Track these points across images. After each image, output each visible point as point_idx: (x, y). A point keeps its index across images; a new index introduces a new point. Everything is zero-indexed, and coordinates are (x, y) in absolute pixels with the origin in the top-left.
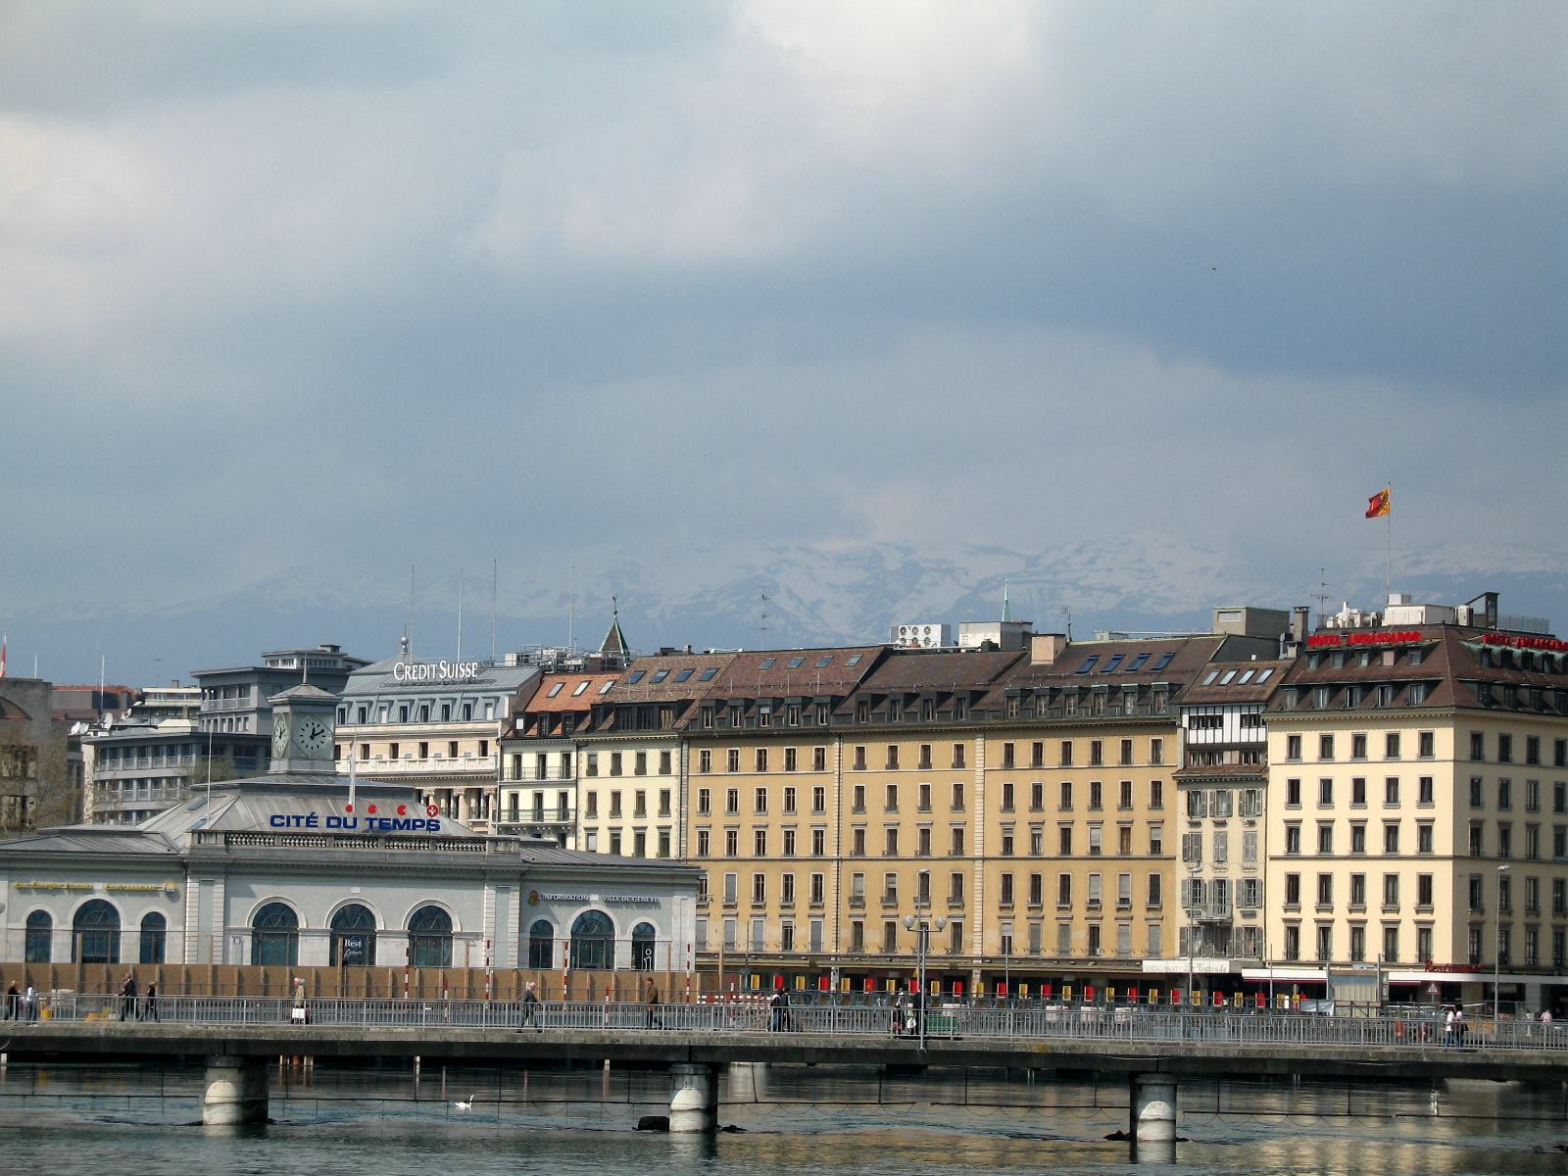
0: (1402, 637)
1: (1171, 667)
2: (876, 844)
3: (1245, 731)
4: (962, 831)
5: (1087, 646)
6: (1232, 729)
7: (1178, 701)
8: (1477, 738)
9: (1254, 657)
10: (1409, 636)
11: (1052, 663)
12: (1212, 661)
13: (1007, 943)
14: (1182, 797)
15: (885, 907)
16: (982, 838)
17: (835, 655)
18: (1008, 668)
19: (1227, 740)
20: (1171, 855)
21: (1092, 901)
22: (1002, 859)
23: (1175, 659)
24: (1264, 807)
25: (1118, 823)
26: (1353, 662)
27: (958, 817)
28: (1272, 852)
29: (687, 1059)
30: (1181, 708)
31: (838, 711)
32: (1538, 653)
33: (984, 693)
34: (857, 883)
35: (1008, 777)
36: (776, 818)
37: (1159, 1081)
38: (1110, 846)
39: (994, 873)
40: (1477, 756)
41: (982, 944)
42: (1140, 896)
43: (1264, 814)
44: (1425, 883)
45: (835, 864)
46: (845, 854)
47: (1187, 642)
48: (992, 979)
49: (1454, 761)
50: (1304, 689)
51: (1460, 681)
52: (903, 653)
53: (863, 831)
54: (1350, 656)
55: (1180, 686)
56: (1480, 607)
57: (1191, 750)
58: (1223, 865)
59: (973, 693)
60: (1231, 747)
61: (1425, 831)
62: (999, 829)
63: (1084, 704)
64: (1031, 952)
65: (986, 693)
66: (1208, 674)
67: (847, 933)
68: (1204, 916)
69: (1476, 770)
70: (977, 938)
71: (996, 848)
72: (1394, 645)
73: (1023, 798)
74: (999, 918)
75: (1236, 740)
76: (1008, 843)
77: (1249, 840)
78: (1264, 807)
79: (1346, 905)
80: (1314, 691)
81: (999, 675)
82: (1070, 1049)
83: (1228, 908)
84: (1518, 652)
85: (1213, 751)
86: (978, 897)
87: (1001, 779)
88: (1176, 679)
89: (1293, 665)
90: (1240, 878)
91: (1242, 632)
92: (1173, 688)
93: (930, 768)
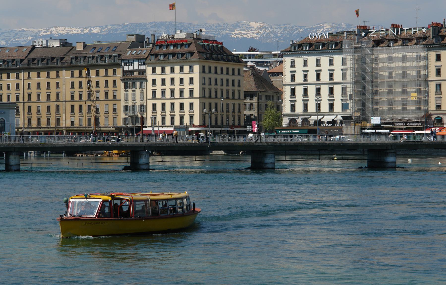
0: (182, 41)
1: (117, 50)
2: (34, 98)
3: (140, 66)
4: (59, 94)
5: (92, 45)
6: (136, 66)
7: (120, 59)
8: (204, 67)
9: (139, 47)
10: (184, 41)
11: (82, 49)
12: (129, 48)
13: (72, 123)
14: (122, 85)
15: (37, 115)
16: (65, 95)
17: (19, 48)
18: (69, 51)
19: (135, 69)
20: (120, 99)
21: (106, 111)
22: (113, 100)
23: (118, 48)
24: (146, 86)
25: (56, 92)
26: (169, 48)
27: (58, 91)
28: (148, 98)
29: (143, 150)
30: (122, 61)
31: (22, 63)
32: (215, 45)
33: (64, 58)
34: (106, 107)
35: (72, 80)
36: (177, 87)
37: (271, 153)
38: (102, 97)
39: (69, 105)
40: (204, 71)
41: (65, 123)
42: (111, 111)
43: (146, 88)
44: (191, 105)
45: (23, 104)
46: (26, 101)
47: (120, 44)
48: (68, 132)
49: (199, 73)
50: (156, 55)
51: (199, 53)
52: (38, 48)
53: (40, 94)
54: (168, 46)
55: (120, 55)
56: (198, 33)
57: (124, 72)
58: (143, 101)
59: (42, 58)
60: (136, 71)
61: (191, 92)
62: (70, 93)
63: (93, 60)
64: (80, 125)
65: (64, 58)
66: (128, 51)
67: (26, 122)
68: (129, 115)
69: (204, 75)
70: (64, 122)
71: (69, 99)
72: (173, 44)
73: (76, 85)
74: (113, 116)
75: (137, 69)
76: (72, 97)
77: (142, 95)
78: (146, 86)
79: (179, 111)
80: (168, 56)
81: (67, 53)
82: (249, 145)
83: (136, 113)
84: (211, 45)
85: (131, 72)
86: (64, 111)
87: (69, 81)
88: (120, 53)
89: (152, 48)
90: (124, 105)
91: (135, 41)
92: (119, 56)
93: (18, 78)
